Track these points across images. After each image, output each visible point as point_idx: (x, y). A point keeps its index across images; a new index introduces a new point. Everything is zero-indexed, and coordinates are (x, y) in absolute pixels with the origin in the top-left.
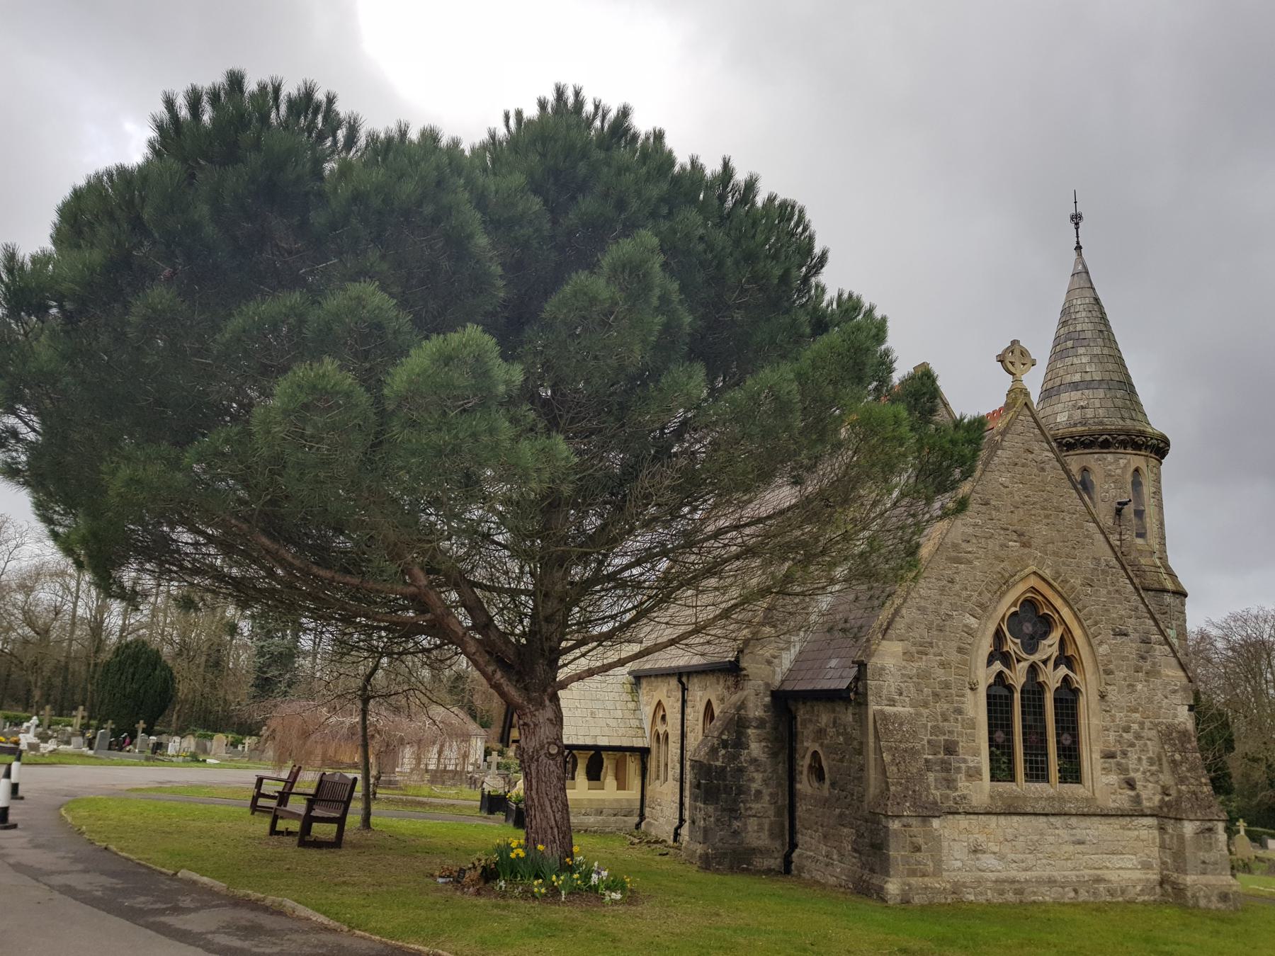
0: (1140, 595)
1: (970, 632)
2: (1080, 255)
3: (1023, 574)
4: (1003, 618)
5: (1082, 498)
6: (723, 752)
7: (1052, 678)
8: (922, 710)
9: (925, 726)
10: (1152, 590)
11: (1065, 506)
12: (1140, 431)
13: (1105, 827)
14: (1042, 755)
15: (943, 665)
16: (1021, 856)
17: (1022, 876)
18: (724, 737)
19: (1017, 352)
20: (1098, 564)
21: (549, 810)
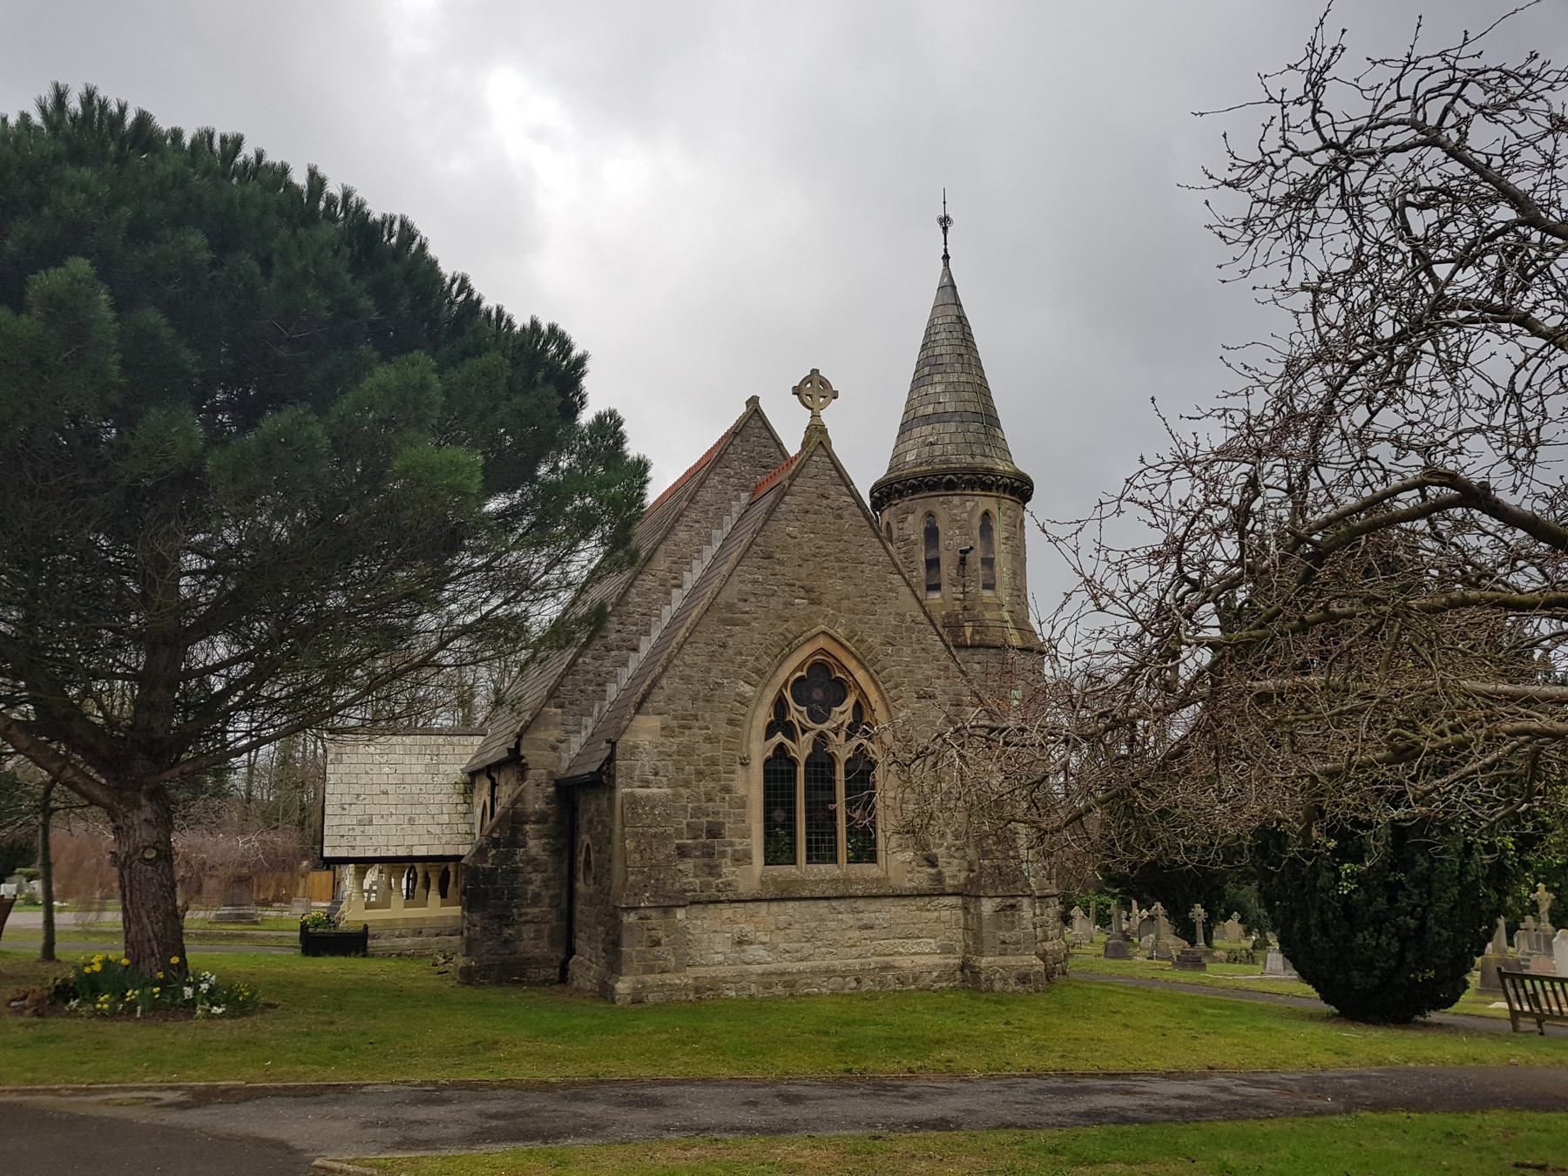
0: (951, 653)
1: (743, 701)
2: (946, 265)
3: (809, 634)
4: (787, 680)
5: (885, 548)
6: (494, 852)
7: (842, 750)
8: (683, 791)
9: (684, 808)
10: (993, 647)
11: (865, 557)
12: (987, 469)
13: (898, 909)
14: (830, 834)
15: (708, 739)
16: (796, 946)
17: (795, 967)
18: (494, 835)
19: (816, 383)
20: (903, 621)
21: (145, 920)
